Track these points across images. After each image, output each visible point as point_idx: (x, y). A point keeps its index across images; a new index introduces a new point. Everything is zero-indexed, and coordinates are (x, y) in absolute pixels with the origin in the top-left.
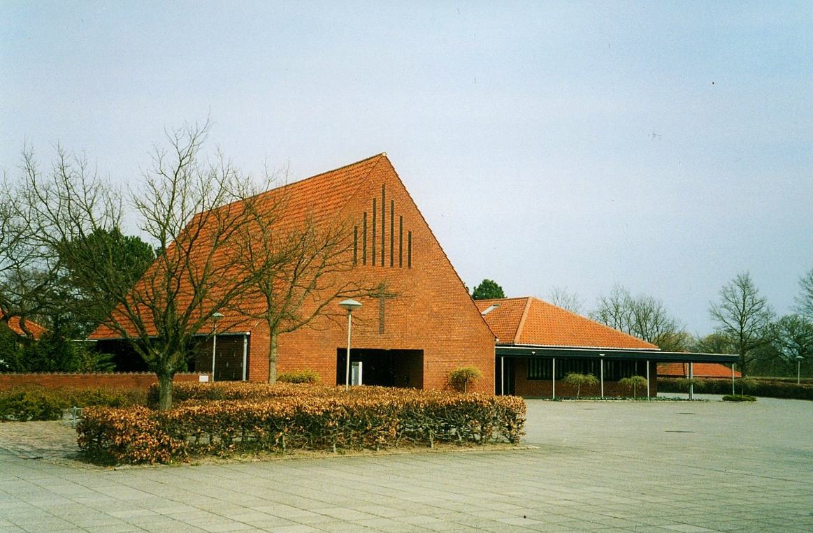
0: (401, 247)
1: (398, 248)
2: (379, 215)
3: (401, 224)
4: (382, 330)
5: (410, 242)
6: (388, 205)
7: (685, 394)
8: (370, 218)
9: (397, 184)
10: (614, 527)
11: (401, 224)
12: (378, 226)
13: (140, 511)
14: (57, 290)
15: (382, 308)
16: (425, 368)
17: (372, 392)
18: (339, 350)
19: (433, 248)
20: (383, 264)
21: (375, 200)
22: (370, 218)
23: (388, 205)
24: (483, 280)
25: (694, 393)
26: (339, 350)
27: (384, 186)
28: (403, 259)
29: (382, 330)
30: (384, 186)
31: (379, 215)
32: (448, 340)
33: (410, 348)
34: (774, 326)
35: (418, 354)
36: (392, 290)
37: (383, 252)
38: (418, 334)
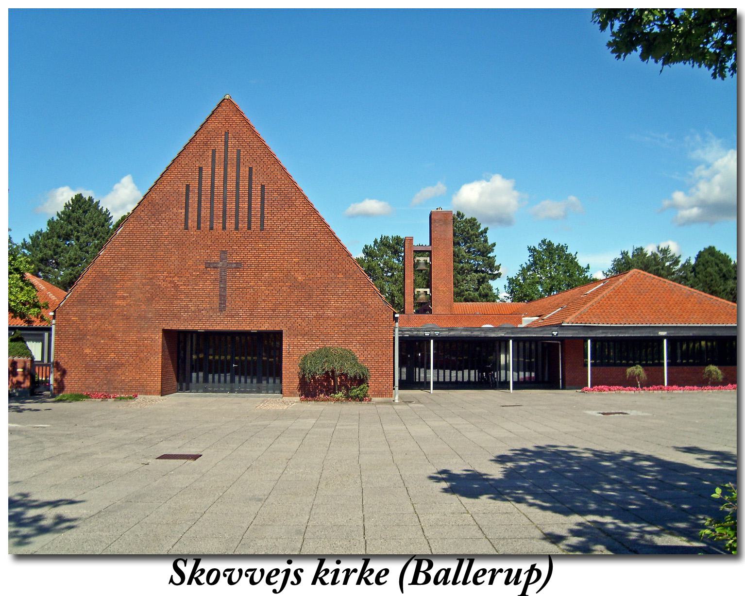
1: (246, 205)
2: (219, 171)
6: (232, 155)
7: (236, 379)
8: (207, 172)
12: (219, 182)
13: (54, 433)
15: (223, 281)
17: (529, 305)
19: (297, 203)
20: (224, 228)
21: (214, 151)
23: (232, 155)
24: (612, 55)
27: (227, 133)
30: (227, 133)
31: (219, 171)
32: (318, 317)
35: (277, 336)
37: (224, 212)
38: (274, 310)
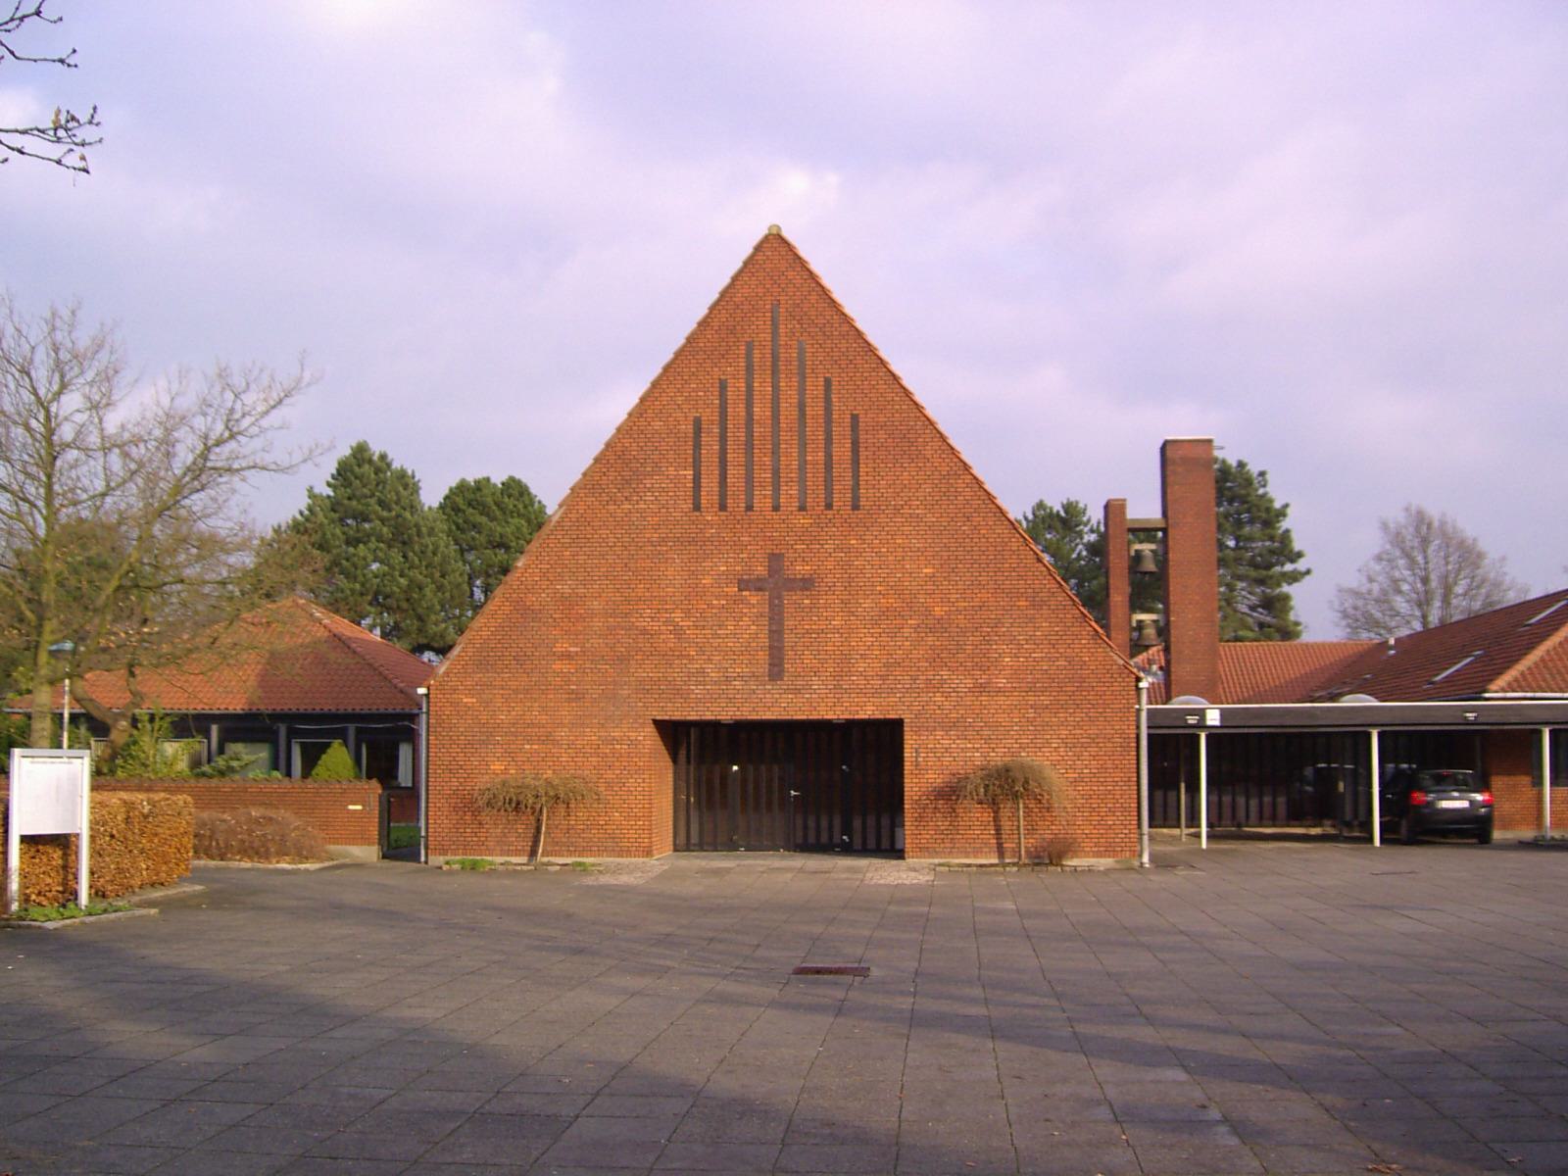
0: (829, 456)
3: (828, 400)
4: (776, 671)
5: (855, 444)
8: (736, 388)
9: (813, 297)
10: (694, 1170)
11: (828, 400)
14: (147, 677)
16: (908, 766)
18: (876, 745)
22: (736, 388)
25: (357, 727)
26: (876, 745)
28: (716, 478)
29: (776, 671)
33: (862, 716)
34: (173, 446)
36: (801, 569)
38: (884, 678)
